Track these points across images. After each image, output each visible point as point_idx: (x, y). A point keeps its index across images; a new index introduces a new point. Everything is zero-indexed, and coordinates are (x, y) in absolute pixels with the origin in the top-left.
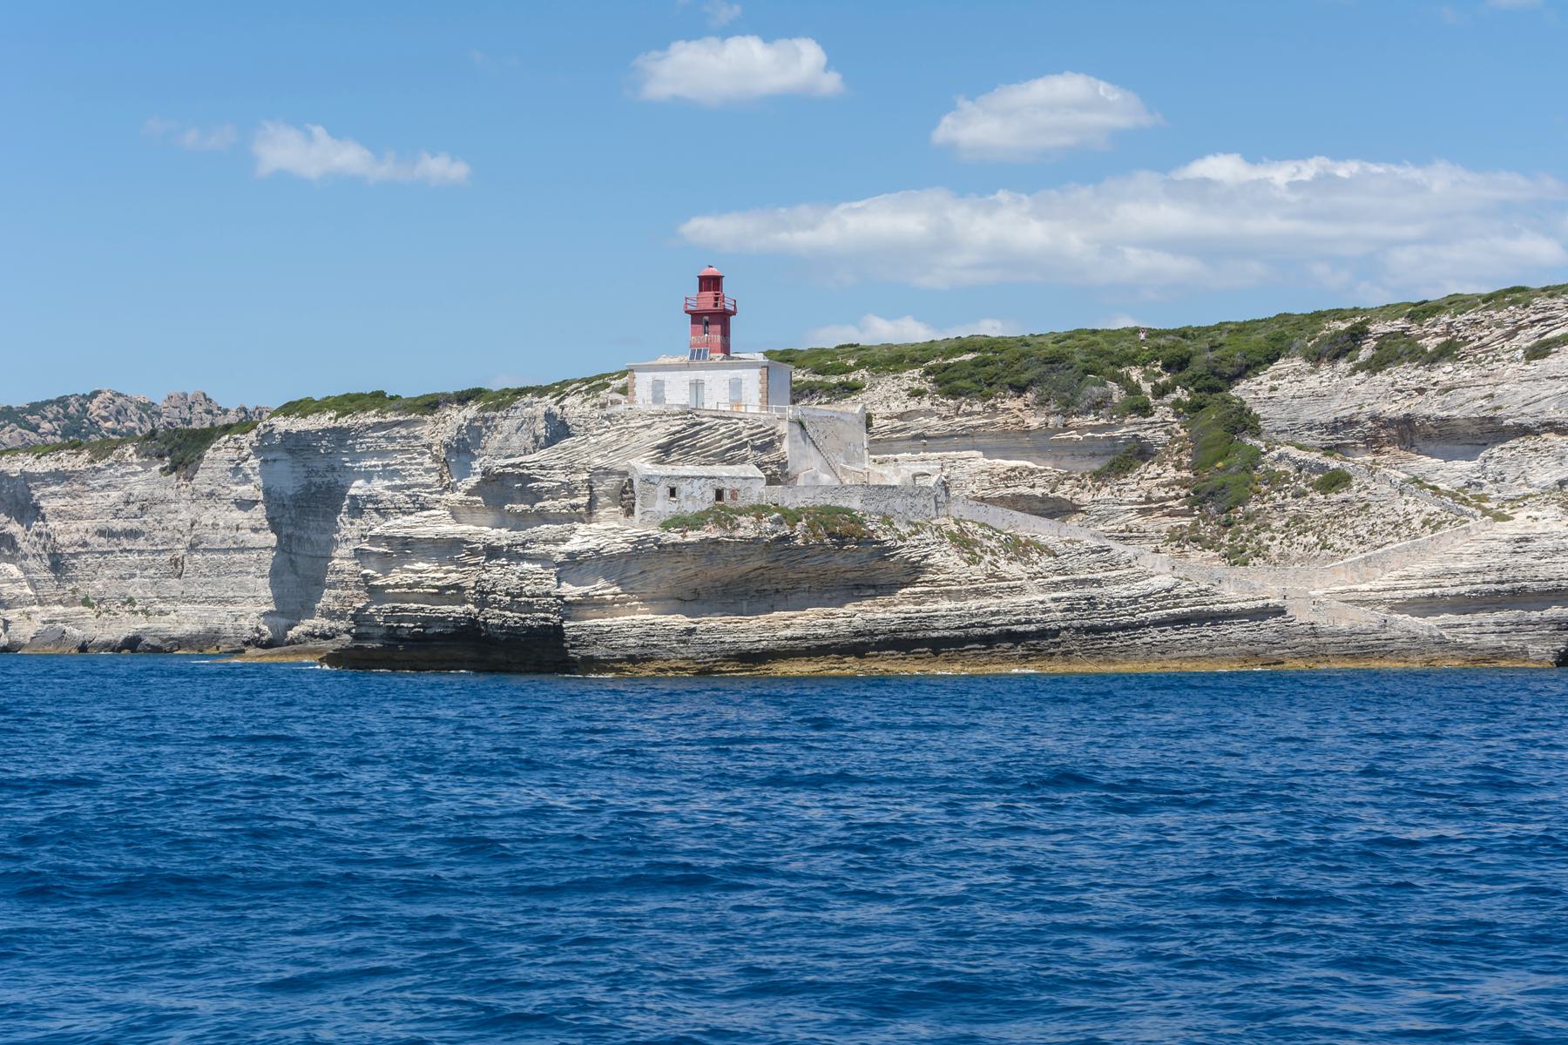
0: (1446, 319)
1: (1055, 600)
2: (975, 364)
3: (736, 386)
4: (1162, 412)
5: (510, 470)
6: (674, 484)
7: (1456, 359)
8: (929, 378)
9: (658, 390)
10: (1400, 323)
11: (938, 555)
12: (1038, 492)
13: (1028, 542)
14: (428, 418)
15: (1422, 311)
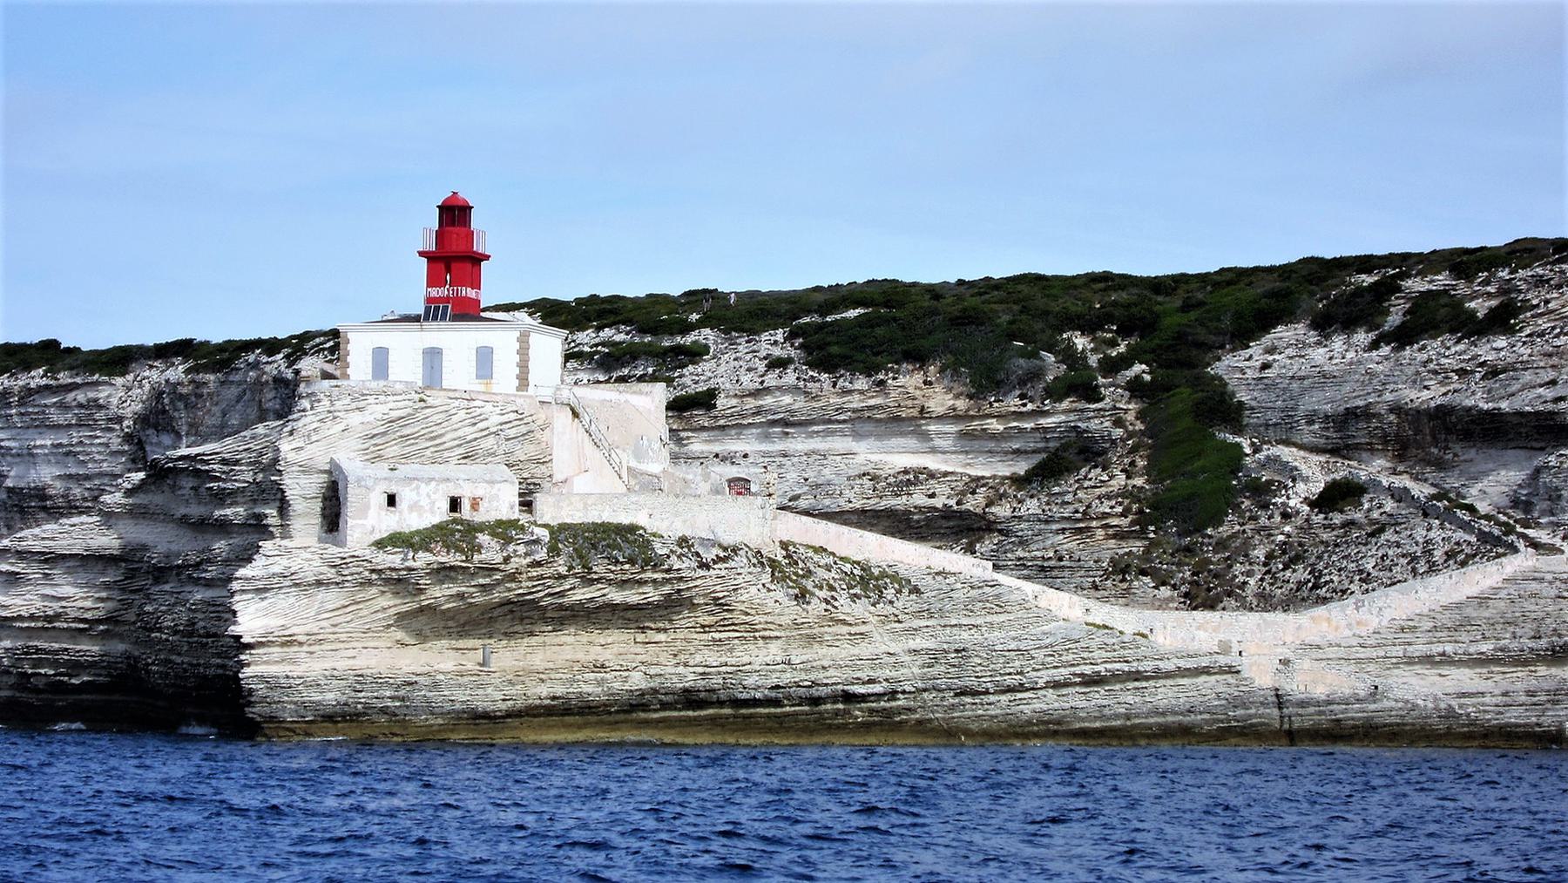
0: (1504, 274)
3: (485, 358)
4: (1113, 393)
6: (393, 489)
7: (1510, 331)
10: (1442, 280)
12: (938, 503)
13: (883, 575)
14: (119, 381)
15: (1465, 262)
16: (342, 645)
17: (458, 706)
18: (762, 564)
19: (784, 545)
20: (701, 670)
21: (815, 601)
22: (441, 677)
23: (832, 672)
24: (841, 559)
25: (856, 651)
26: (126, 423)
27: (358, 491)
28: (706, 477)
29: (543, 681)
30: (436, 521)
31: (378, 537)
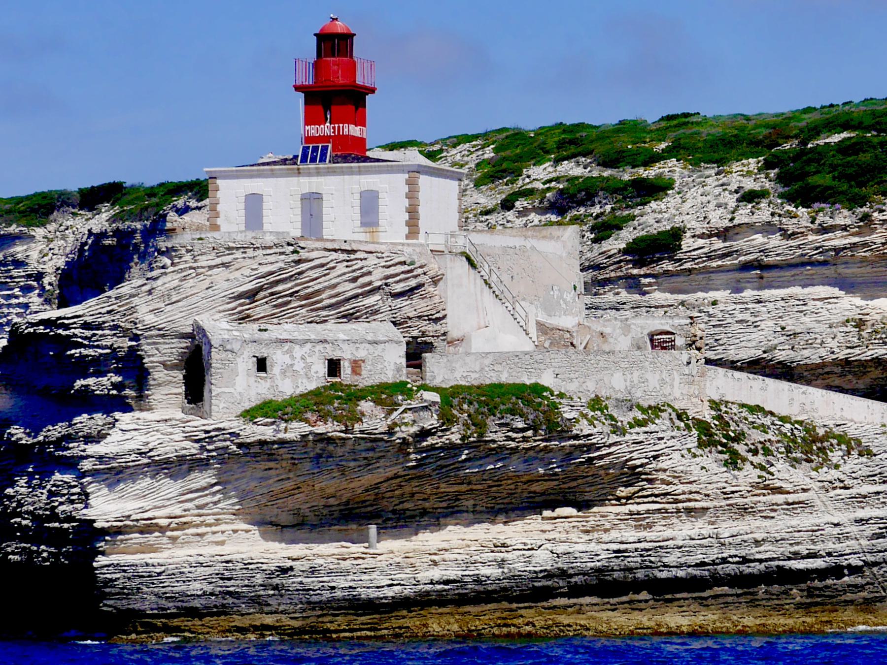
1: (860, 521)
2: (843, 148)
3: (369, 206)
5: (41, 329)
6: (263, 352)
8: (773, 173)
9: (254, 205)
11: (676, 455)
13: (828, 435)
14: (39, 232)
16: (208, 529)
17: (339, 594)
18: (688, 427)
19: (715, 405)
20: (615, 547)
21: (748, 466)
22: (321, 561)
23: (765, 547)
24: (781, 419)
25: (794, 522)
26: (46, 281)
27: (224, 355)
28: (626, 329)
29: (435, 563)
30: (312, 386)
31: (247, 406)
